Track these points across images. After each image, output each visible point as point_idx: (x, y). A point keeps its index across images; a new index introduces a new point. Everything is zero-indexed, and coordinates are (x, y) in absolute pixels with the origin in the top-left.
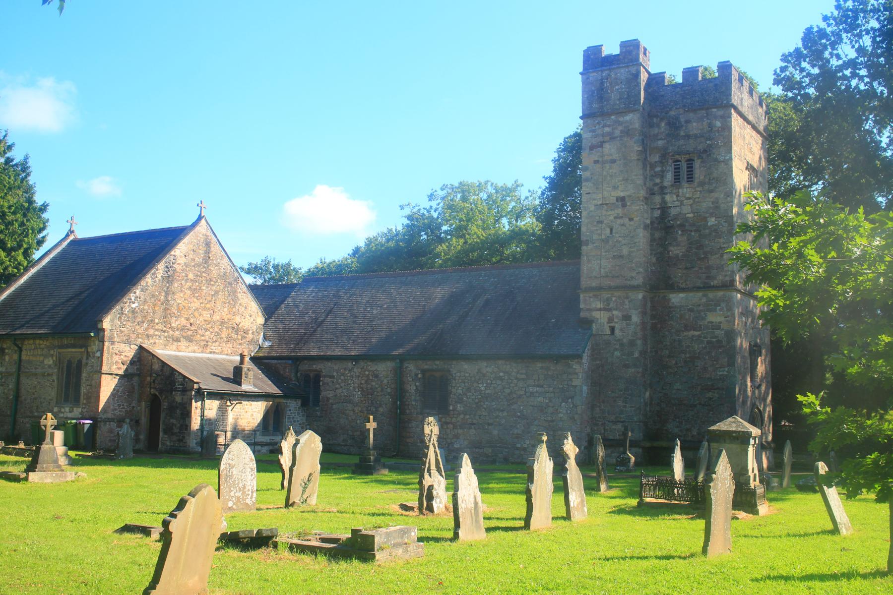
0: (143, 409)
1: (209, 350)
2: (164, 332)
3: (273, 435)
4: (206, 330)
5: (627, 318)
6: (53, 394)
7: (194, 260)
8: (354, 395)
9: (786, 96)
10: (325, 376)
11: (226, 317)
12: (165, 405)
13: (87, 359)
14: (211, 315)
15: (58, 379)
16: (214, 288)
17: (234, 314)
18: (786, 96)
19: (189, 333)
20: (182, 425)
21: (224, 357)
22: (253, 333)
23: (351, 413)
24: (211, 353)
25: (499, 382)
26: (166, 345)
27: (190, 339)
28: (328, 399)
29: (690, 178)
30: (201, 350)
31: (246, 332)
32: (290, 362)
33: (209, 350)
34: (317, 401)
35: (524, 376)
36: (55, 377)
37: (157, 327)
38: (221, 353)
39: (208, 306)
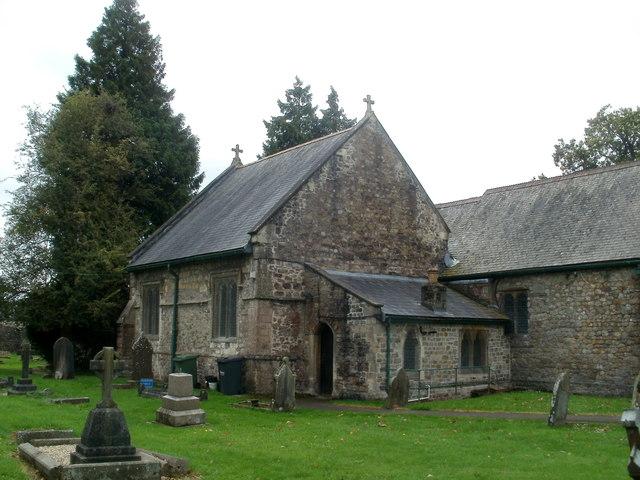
0: (311, 343)
1: (388, 271)
2: (334, 248)
3: (474, 373)
4: (384, 246)
6: (209, 327)
7: (363, 162)
8: (576, 319)
9: (91, 450)
10: (533, 296)
11: (405, 232)
12: (337, 337)
13: (242, 282)
14: (389, 229)
15: (213, 309)
16: (390, 196)
17: (415, 228)
18: (91, 450)
19: (364, 250)
20: (360, 364)
21: (406, 279)
22: (437, 250)
23: (573, 340)
24: (390, 274)
26: (337, 264)
27: (364, 257)
28: (539, 324)
30: (377, 271)
31: (429, 249)
32: (487, 280)
33: (388, 271)
34: (524, 327)
36: (210, 307)
37: (325, 241)
38: (402, 274)
39: (384, 217)
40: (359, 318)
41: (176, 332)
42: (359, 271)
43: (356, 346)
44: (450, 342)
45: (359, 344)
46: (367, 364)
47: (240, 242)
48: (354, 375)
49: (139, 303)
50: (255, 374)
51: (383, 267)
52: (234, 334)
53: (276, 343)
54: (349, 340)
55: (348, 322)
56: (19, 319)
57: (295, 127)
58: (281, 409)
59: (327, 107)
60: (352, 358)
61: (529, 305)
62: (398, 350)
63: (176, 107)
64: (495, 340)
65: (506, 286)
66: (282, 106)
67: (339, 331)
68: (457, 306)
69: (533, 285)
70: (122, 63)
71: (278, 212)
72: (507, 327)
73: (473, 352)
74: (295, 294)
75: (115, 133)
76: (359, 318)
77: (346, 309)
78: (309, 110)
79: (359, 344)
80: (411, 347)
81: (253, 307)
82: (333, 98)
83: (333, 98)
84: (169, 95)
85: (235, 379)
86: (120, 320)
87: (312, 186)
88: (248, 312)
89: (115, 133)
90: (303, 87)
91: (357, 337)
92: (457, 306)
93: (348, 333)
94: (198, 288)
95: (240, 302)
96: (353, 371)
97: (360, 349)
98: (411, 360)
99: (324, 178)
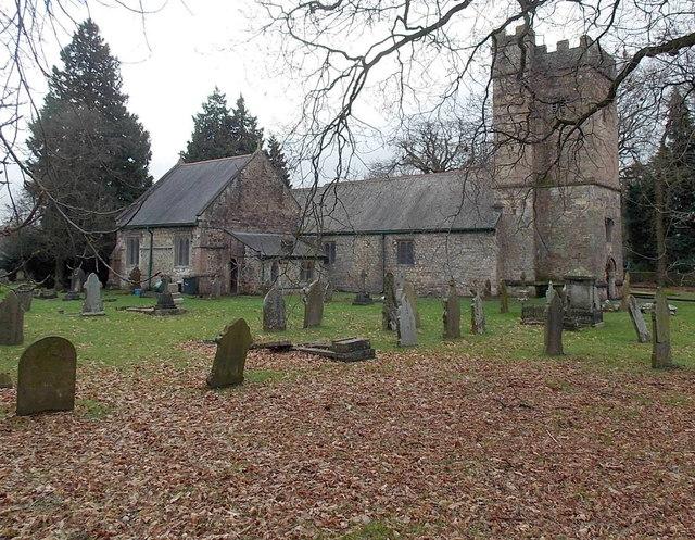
0: (226, 268)
41: (151, 263)
42: (252, 233)
44: (294, 270)
47: (193, 220)
49: (124, 246)
50: (202, 285)
51: (264, 228)
52: (187, 264)
53: (210, 269)
59: (236, 108)
61: (79, 371)
62: (268, 272)
63: (131, 107)
64: (318, 265)
65: (325, 239)
66: (205, 106)
68: (301, 249)
70: (89, 72)
71: (211, 204)
72: (326, 260)
73: (307, 273)
74: (220, 244)
75: (86, 122)
78: (224, 111)
80: (274, 269)
81: (198, 250)
82: (240, 102)
83: (240, 102)
84: (124, 98)
85: (192, 287)
86: (112, 256)
87: (228, 190)
88: (195, 252)
89: (86, 122)
90: (220, 94)
92: (301, 249)
94: (166, 240)
95: (190, 249)
98: (275, 277)
99: (234, 185)
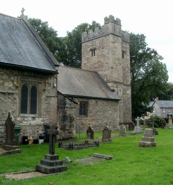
5: (120, 90)
20: (70, 125)
25: (101, 106)
29: (95, 55)
35: (107, 105)
40: (71, 108)
43: (69, 118)
45: (70, 118)
46: (73, 125)
48: (68, 130)
54: (66, 116)
55: (66, 109)
56: (5, 133)
57: (106, 19)
58: (110, 139)
60: (67, 123)
63: (136, 34)
67: (62, 113)
69: (92, 102)
76: (71, 108)
77: (65, 104)
79: (70, 118)
91: (70, 115)
93: (65, 113)
96: (67, 128)
97: (71, 119)
